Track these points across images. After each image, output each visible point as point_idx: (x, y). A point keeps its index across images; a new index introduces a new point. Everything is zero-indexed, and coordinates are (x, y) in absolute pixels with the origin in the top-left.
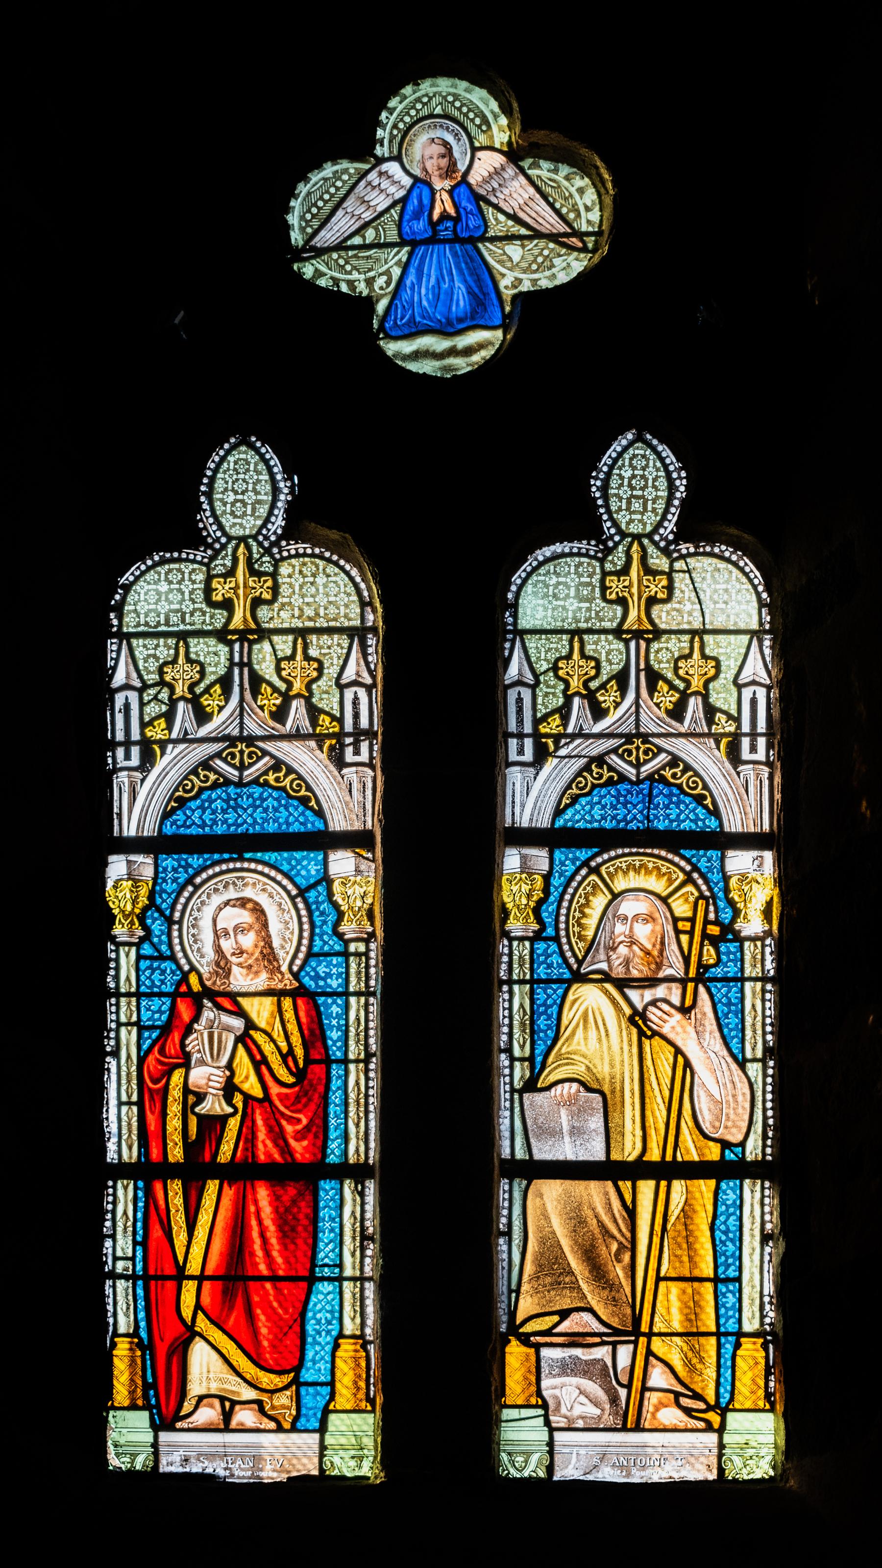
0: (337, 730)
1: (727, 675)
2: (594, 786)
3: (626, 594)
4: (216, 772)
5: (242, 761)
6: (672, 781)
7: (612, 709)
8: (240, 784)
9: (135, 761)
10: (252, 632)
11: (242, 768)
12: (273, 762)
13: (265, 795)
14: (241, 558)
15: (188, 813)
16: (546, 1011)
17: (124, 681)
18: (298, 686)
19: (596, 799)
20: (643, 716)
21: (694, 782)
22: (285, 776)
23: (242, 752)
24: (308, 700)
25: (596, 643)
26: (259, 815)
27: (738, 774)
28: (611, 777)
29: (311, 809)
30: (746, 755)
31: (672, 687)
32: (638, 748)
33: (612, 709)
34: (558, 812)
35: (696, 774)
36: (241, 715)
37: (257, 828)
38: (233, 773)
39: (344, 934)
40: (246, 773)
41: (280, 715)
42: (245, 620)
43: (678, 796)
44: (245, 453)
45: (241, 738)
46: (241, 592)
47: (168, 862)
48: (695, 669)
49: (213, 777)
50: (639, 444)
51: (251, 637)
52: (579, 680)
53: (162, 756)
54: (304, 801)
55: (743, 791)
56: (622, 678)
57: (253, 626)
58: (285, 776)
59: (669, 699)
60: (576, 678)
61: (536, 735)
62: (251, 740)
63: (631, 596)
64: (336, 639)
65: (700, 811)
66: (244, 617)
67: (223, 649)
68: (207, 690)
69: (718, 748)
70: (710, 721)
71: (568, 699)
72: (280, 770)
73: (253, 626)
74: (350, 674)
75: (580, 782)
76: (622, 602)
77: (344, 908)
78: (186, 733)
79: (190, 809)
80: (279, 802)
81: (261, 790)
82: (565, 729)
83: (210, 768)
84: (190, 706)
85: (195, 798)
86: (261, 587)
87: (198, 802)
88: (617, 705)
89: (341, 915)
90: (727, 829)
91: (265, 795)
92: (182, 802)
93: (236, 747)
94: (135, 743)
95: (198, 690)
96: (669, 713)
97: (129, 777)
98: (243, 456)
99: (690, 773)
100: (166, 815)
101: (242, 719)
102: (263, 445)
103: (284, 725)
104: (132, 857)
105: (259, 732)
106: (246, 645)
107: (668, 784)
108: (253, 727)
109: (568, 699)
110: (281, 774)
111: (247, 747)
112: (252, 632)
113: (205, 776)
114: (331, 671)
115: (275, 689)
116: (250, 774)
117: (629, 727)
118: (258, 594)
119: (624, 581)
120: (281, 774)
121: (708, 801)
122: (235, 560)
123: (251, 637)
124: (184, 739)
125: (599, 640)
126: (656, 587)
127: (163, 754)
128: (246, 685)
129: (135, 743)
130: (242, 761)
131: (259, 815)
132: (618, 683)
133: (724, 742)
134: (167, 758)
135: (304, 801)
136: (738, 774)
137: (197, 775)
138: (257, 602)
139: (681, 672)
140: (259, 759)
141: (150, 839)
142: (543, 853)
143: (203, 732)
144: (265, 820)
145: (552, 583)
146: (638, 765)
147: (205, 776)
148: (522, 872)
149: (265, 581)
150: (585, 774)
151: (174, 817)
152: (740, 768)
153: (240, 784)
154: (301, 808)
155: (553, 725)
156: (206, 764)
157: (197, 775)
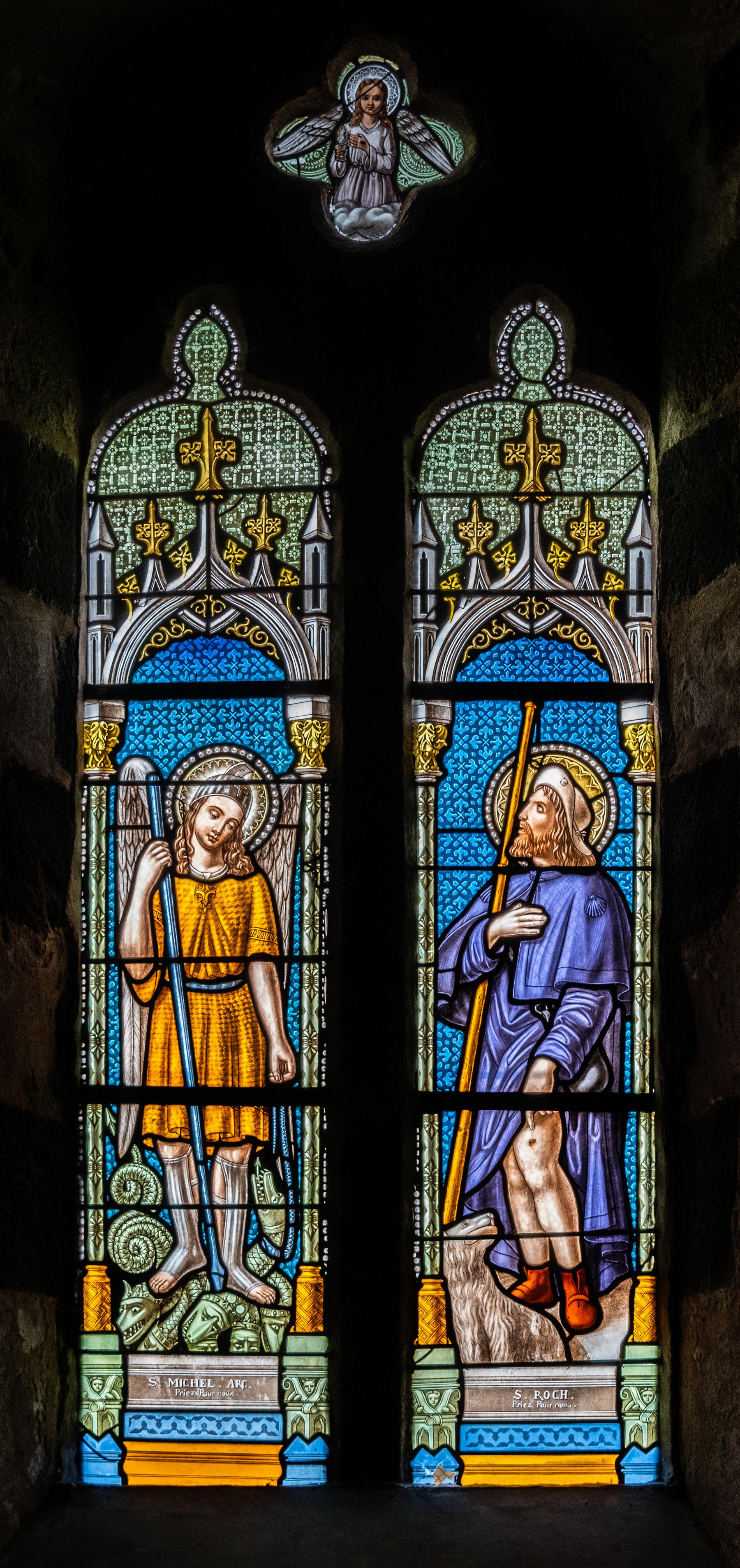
0: (621, 587)
1: (293, 534)
2: (493, 643)
3: (523, 460)
4: (509, 626)
5: (531, 614)
6: (239, 635)
7: (508, 570)
8: (532, 636)
9: (107, 615)
10: (218, 492)
11: (209, 619)
12: (238, 614)
13: (550, 648)
14: (206, 423)
15: (157, 663)
16: (452, 852)
17: (637, 539)
18: (262, 542)
19: (495, 655)
20: (537, 576)
21: (260, 636)
22: (250, 627)
23: (208, 604)
24: (271, 555)
25: (438, 505)
26: (545, 667)
27: (626, 630)
28: (510, 633)
29: (272, 658)
30: (633, 612)
31: (564, 547)
32: (531, 605)
33: (508, 570)
34: (460, 667)
35: (263, 628)
36: (208, 570)
37: (270, 676)
38: (524, 625)
39: (633, 777)
40: (213, 624)
41: (244, 569)
42: (211, 482)
43: (571, 652)
44: (535, 324)
45: (531, 593)
46: (531, 456)
47: (135, 706)
48: (587, 530)
49: (505, 631)
50: (206, 321)
51: (217, 497)
52: (478, 542)
53: (455, 610)
54: (264, 651)
55: (631, 648)
56: (516, 539)
57: (219, 487)
58: (250, 627)
59: (559, 558)
60: (263, 536)
61: (439, 594)
62: (542, 595)
63: (527, 460)
64: (625, 501)
65: (592, 665)
66: (534, 480)
67: (513, 509)
68: (498, 547)
69: (608, 607)
70: (600, 579)
71: (467, 559)
72: (245, 621)
73: (219, 487)
74: (636, 534)
75: (159, 637)
76: (519, 467)
77: (635, 753)
78: (585, 586)
79: (158, 659)
80: (564, 655)
81: (225, 641)
82: (141, 587)
83: (179, 621)
84: (483, 562)
85: (488, 649)
86: (550, 453)
87: (167, 654)
88: (189, 565)
89: (298, 756)
90: (615, 680)
91: (550, 648)
92: (474, 655)
93: (526, 600)
94: (108, 597)
95: (492, 546)
96: (238, 569)
97: (102, 630)
98: (207, 328)
99: (581, 629)
100: (137, 665)
101: (209, 575)
102: (552, 318)
103: (249, 579)
104: (105, 703)
105: (548, 587)
106: (213, 506)
107: (562, 641)
108: (543, 584)
109: (467, 559)
110: (570, 627)
111: (214, 599)
112: (540, 494)
113: (176, 629)
114: (616, 531)
115: (240, 545)
116: (541, 624)
117: (525, 585)
118: (547, 460)
119: (521, 448)
120: (570, 627)
121: (597, 655)
122: (201, 426)
123: (217, 497)
124: (158, 594)
125: (442, 502)
126: (550, 456)
127: (457, 608)
128: (537, 543)
129: (108, 597)
130: (531, 614)
131: (545, 667)
132: (190, 545)
133: (613, 599)
134: (139, 611)
135: (589, 653)
136: (626, 630)
137: (169, 627)
138: (221, 464)
139: (573, 534)
140: (547, 613)
141: (120, 687)
142: (119, 704)
143: (497, 585)
144: (182, 672)
145: (131, 449)
146: (532, 620)
147: (176, 629)
148: (312, 719)
149: (229, 444)
150: (485, 630)
151: (144, 668)
152: (628, 625)
153: (532, 636)
154: (262, 659)
155: (454, 583)
156: (499, 618)
157: (169, 627)
